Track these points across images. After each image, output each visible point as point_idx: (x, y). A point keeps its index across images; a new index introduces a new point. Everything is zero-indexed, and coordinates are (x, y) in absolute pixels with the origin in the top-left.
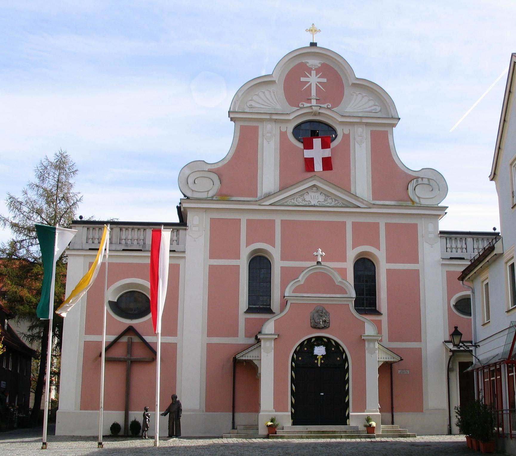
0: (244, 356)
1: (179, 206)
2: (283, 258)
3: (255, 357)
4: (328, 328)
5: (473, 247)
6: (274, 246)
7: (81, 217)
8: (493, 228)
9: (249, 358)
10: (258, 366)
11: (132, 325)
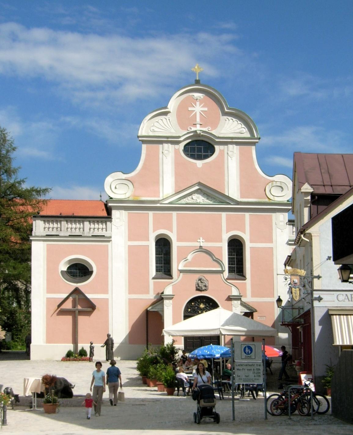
1: (106, 203)
2: (251, 241)
3: (243, 310)
6: (172, 232)
7: (61, 214)
10: (162, 314)
11: (77, 287)
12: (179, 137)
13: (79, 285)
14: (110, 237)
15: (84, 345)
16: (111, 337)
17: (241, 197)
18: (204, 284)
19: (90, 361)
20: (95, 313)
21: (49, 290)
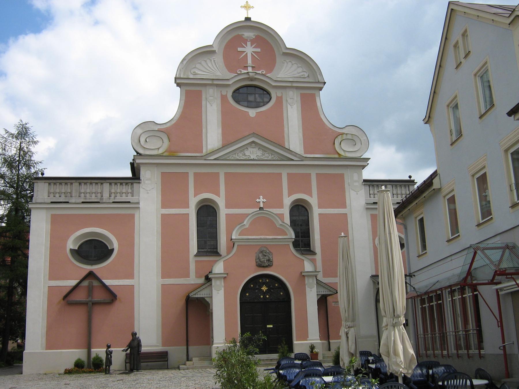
1: (132, 162)
3: (207, 294)
6: (219, 196)
8: (408, 176)
9: (201, 296)
10: (209, 302)
11: (91, 270)
13: (94, 268)
15: (99, 352)
16: (137, 336)
17: (305, 153)
18: (267, 258)
19: (106, 373)
20: (117, 304)
21: (52, 276)
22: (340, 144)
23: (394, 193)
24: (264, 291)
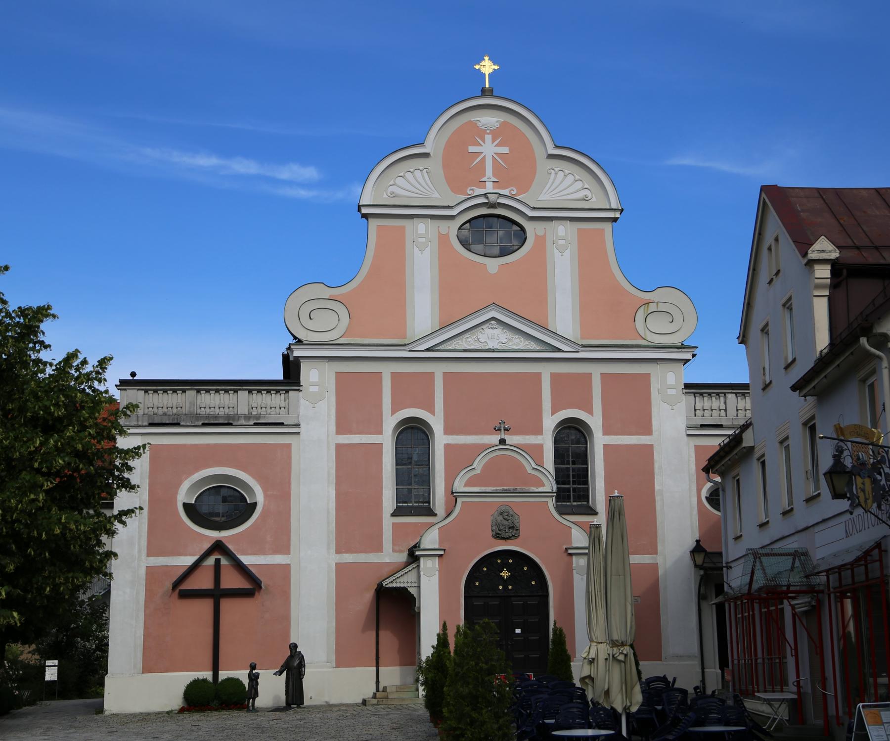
0: (395, 581)
1: (286, 353)
2: (606, 432)
3: (411, 582)
4: (517, 537)
5: (695, 407)
6: (433, 413)
9: (402, 585)
12: (449, 207)
14: (298, 425)
22: (645, 321)
23: (738, 409)
24: (505, 577)
